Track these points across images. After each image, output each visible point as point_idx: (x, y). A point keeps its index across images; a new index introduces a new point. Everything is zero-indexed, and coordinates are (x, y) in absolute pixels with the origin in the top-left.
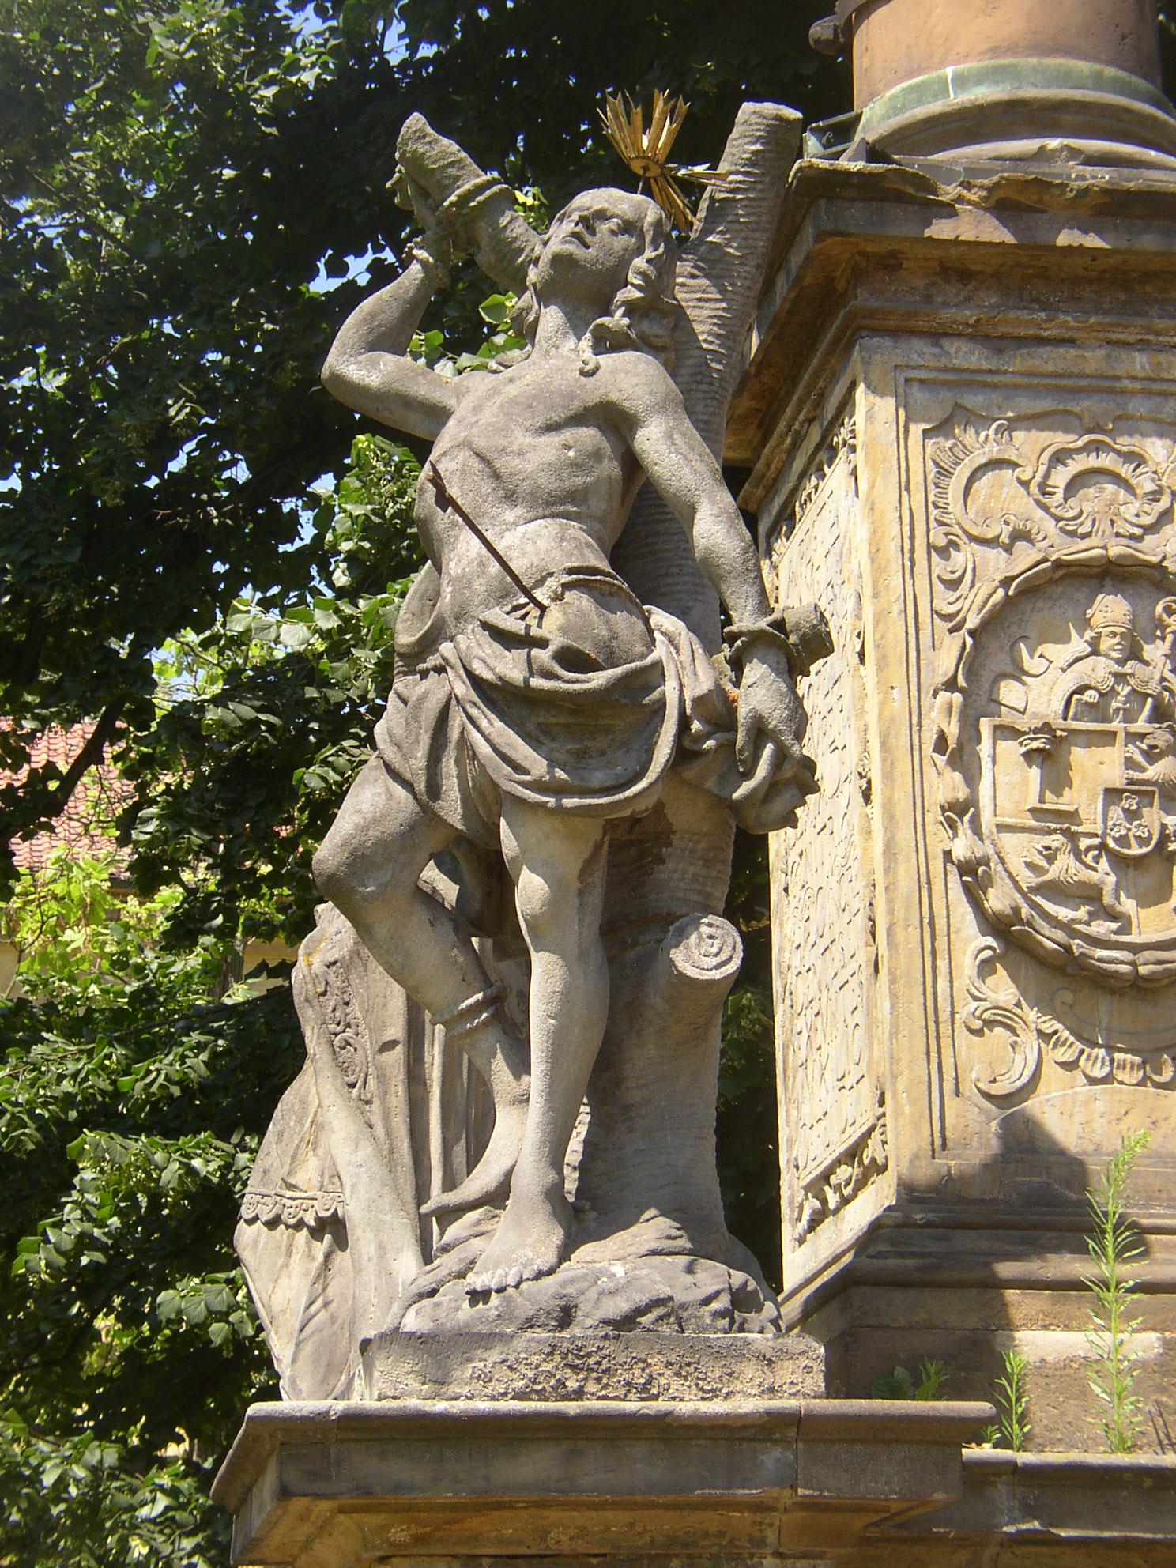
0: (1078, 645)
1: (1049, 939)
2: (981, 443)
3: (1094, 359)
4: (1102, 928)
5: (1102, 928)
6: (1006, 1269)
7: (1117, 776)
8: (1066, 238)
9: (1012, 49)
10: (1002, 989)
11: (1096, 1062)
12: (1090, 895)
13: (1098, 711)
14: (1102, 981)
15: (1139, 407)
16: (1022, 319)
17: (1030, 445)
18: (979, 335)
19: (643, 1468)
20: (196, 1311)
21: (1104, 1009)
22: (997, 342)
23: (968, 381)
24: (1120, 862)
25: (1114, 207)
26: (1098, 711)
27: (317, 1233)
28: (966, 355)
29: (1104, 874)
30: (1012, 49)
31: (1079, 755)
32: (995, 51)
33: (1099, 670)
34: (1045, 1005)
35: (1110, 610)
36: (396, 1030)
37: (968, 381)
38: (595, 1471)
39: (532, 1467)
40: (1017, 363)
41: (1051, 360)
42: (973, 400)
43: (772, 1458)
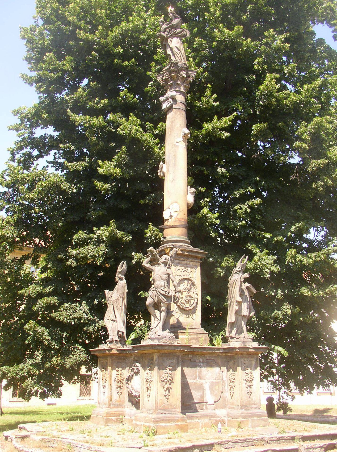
0: (184, 284)
1: (181, 307)
2: (178, 268)
3: (186, 262)
4: (184, 306)
5: (184, 306)
6: (178, 331)
7: (186, 295)
8: (185, 253)
9: (179, 235)
10: (177, 310)
11: (183, 316)
12: (184, 303)
13: (185, 290)
14: (184, 310)
15: (188, 266)
16: (181, 259)
17: (181, 268)
18: (178, 260)
19: (173, 348)
20: (55, 316)
21: (184, 312)
22: (179, 260)
23: (178, 263)
24: (186, 301)
25: (189, 251)
26: (185, 290)
27: (112, 321)
28: (177, 261)
29: (185, 302)
30: (179, 235)
31: (183, 293)
32: (178, 235)
33: (185, 286)
34: (180, 311)
35: (186, 282)
36: (121, 305)
37: (178, 263)
38: (170, 348)
39: (167, 348)
40: (181, 262)
41: (183, 262)
42: (177, 264)
43: (180, 347)
